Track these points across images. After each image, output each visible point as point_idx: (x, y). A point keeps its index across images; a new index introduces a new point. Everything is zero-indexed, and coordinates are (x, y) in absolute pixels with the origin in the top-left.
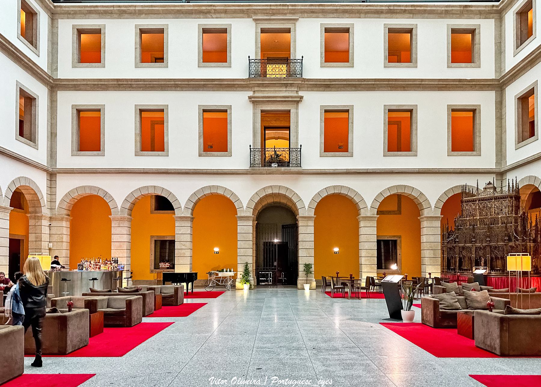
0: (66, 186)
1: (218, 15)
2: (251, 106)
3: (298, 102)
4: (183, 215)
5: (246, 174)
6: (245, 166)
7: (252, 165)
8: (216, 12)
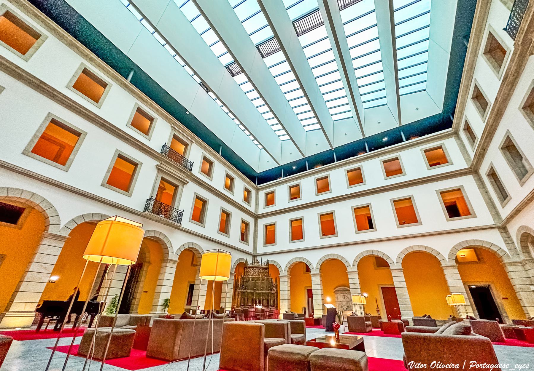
1: (151, 108)
2: (156, 171)
3: (185, 184)
4: (58, 234)
5: (139, 215)
6: (140, 208)
7: (146, 209)
8: (154, 108)
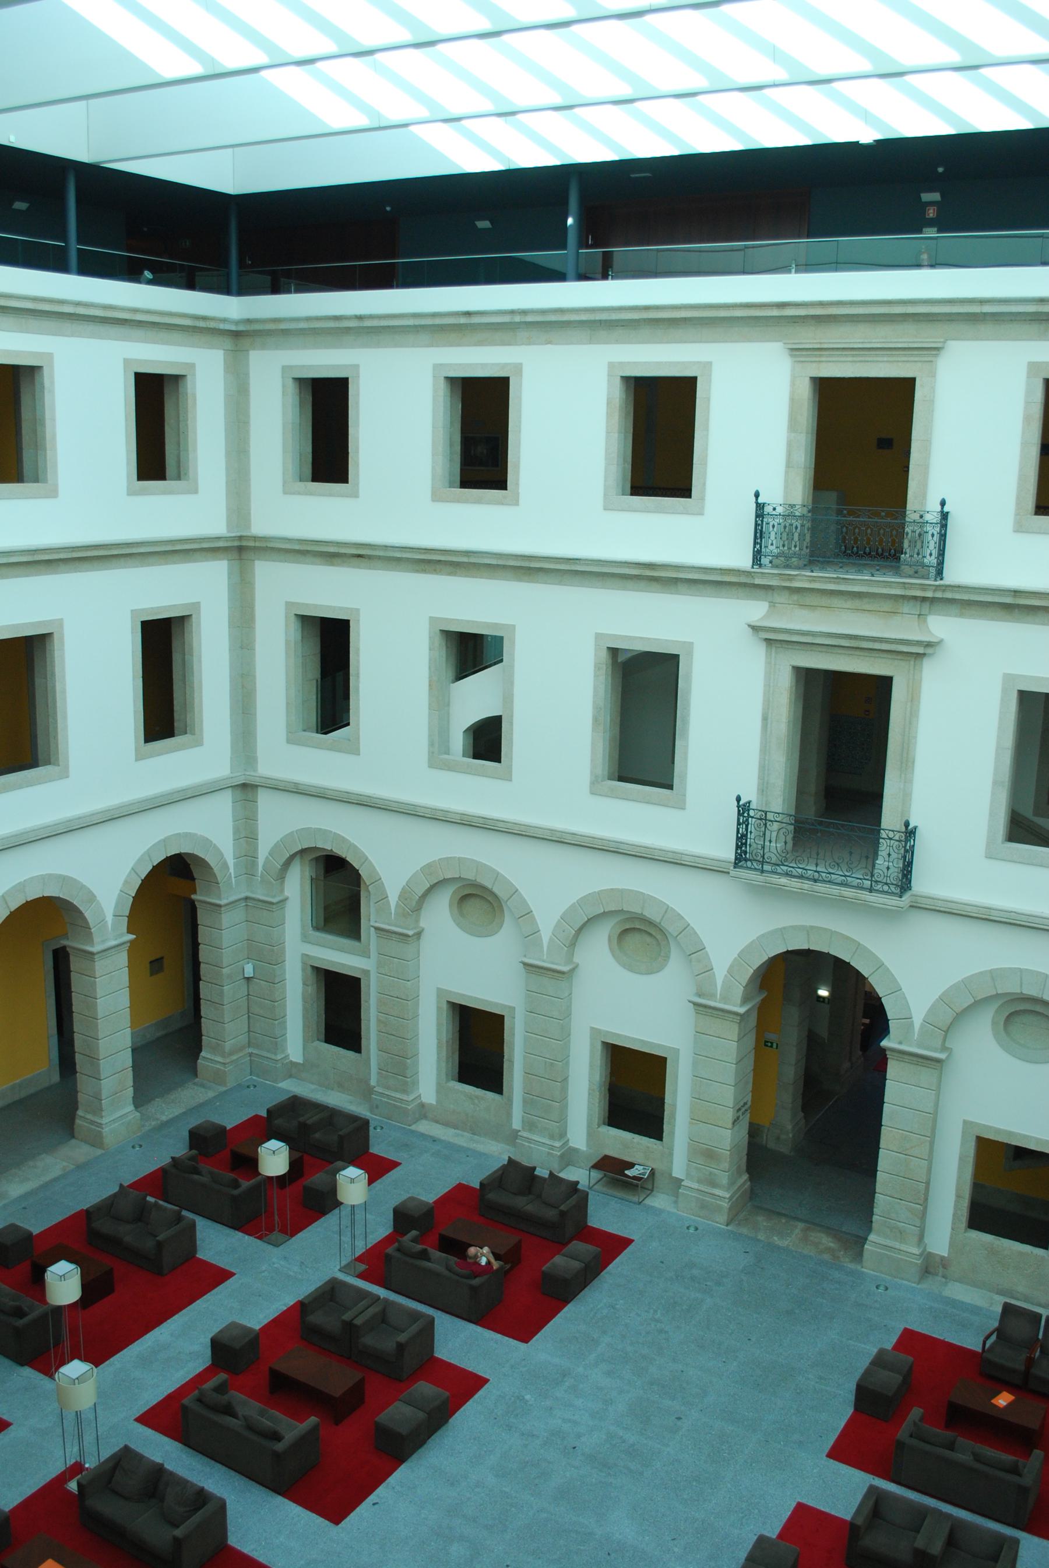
0: (281, 823)
